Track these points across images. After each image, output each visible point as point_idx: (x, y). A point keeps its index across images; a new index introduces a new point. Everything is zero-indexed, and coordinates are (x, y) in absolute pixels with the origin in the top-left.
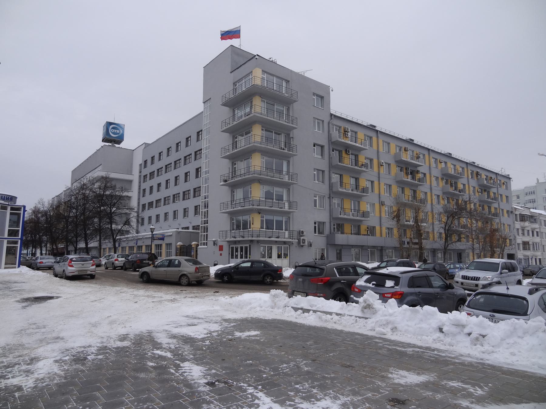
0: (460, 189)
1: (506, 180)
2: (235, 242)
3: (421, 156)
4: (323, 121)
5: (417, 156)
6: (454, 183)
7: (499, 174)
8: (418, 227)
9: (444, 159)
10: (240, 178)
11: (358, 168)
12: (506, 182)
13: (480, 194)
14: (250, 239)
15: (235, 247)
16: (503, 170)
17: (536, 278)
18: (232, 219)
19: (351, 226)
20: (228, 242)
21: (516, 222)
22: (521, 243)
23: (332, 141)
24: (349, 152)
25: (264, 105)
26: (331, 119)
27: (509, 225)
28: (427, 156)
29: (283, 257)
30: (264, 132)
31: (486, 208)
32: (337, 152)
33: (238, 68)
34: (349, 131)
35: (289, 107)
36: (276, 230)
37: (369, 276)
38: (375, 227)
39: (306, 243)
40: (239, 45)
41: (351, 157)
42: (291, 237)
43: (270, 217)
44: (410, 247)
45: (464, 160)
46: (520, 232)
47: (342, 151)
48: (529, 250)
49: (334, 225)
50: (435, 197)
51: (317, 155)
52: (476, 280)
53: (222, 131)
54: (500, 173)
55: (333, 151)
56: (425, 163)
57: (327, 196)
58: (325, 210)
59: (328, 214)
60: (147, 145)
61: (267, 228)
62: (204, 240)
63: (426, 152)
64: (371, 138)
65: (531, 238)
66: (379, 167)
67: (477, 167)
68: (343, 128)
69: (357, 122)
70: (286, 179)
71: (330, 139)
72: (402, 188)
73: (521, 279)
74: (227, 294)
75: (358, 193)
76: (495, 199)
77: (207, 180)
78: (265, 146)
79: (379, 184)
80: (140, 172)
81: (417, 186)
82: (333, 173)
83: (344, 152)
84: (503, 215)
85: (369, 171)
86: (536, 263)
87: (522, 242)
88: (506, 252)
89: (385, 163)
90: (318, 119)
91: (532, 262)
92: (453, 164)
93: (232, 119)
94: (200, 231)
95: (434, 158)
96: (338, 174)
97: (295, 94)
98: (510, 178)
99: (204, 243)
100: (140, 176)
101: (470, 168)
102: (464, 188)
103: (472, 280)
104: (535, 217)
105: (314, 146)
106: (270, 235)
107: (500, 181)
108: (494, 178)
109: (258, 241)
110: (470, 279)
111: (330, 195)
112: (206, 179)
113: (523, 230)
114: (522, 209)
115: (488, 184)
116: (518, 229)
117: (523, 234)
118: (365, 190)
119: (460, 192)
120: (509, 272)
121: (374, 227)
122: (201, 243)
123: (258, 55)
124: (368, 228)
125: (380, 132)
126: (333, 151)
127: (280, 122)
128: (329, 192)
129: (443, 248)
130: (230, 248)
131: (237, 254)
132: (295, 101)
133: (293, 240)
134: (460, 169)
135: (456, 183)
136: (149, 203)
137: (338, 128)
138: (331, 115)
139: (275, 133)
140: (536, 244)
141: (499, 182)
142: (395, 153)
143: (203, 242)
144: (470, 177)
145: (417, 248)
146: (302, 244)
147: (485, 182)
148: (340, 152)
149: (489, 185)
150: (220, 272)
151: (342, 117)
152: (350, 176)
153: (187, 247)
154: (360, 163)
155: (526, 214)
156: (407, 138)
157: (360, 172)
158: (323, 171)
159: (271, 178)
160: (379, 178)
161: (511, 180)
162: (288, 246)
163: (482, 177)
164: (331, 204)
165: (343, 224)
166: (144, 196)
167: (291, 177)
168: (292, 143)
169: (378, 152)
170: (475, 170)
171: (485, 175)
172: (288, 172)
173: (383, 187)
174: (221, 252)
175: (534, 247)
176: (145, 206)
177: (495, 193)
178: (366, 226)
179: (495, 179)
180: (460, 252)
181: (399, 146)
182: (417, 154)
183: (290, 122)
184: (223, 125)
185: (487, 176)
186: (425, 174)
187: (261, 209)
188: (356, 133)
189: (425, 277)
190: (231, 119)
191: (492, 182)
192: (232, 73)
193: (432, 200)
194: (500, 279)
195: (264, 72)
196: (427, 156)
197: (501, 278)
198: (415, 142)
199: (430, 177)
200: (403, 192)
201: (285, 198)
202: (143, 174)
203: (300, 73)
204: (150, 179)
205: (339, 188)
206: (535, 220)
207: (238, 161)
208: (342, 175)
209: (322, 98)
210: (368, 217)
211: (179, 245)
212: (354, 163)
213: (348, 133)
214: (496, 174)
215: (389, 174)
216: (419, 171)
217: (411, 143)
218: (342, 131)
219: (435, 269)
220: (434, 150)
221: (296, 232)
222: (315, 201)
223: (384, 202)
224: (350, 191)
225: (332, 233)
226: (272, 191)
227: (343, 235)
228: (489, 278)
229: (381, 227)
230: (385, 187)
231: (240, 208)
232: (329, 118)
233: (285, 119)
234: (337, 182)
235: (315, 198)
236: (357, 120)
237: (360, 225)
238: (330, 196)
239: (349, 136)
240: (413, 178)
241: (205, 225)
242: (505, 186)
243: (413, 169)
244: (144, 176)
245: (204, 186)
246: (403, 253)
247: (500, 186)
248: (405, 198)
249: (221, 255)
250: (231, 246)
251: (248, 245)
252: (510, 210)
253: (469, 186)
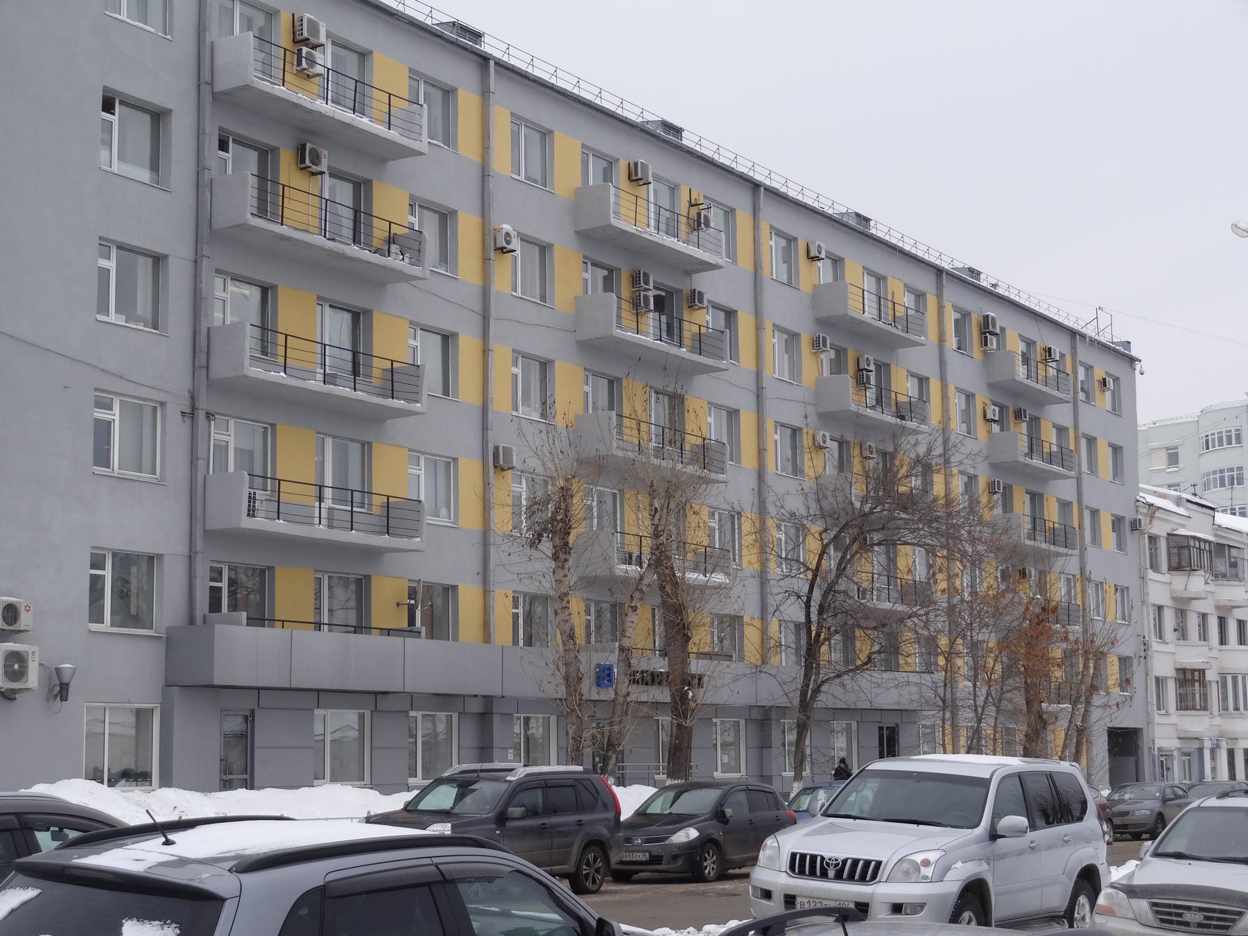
0: (901, 399)
1: (1116, 368)
3: (715, 216)
5: (694, 211)
6: (872, 367)
7: (1083, 336)
8: (668, 588)
9: (827, 241)
11: (366, 255)
12: (1116, 380)
13: (996, 428)
16: (1104, 321)
17: (1156, 854)
19: (319, 581)
21: (1151, 574)
22: (1172, 673)
23: (220, 86)
24: (316, 159)
27: (1121, 590)
28: (743, 219)
31: (1022, 504)
32: (253, 156)
37: (31, 893)
38: (455, 588)
39: (33, 678)
44: (621, 700)
45: (926, 257)
46: (1169, 620)
47: (275, 150)
48: (1205, 709)
49: (216, 575)
50: (775, 437)
51: (121, 158)
52: (863, 879)
54: (1090, 331)
55: (223, 146)
56: (732, 254)
58: (160, 483)
63: (740, 200)
64: (448, 93)
65: (1215, 653)
66: (486, 260)
67: (990, 294)
68: (285, 19)
72: (611, 382)
73: (1101, 862)
75: (359, 395)
76: (1063, 457)
79: (486, 351)
81: (689, 371)
82: (218, 271)
83: (286, 159)
84: (1096, 539)
85: (428, 274)
86: (1232, 775)
87: (1178, 670)
88: (1100, 722)
89: (525, 240)
91: (1214, 769)
92: (871, 273)
95: (779, 233)
96: (250, 282)
98: (1132, 360)
101: (953, 295)
102: (921, 398)
103: (839, 876)
104: (1234, 552)
105: (108, 106)
107: (1089, 369)
108: (1062, 356)
110: (831, 873)
111: (193, 398)
113: (1181, 614)
114: (1181, 511)
115: (1034, 384)
116: (1160, 608)
117: (1182, 632)
118: (706, 455)
119: (903, 418)
120: (1033, 827)
121: (449, 591)
124: (412, 593)
125: (500, 64)
128: (188, 386)
129: (796, 702)
134: (907, 300)
135: (883, 369)
137: (260, 20)
140: (1235, 679)
141: (1081, 373)
142: (577, 190)
144: (952, 341)
145: (656, 705)
147: (1021, 371)
148: (266, 155)
149: (1040, 387)
154: (380, 231)
155: (1194, 538)
156: (849, 211)
157: (379, 280)
158: (158, 260)
160: (485, 317)
161: (1138, 367)
163: (1008, 348)
164: (201, 453)
165: (271, 569)
169: (485, 174)
170: (979, 308)
171: (1023, 339)
173: (505, 369)
175: (1225, 698)
177: (1066, 429)
178: (406, 584)
179: (1068, 359)
180: (889, 722)
181: (599, 156)
182: (691, 205)
185: (1030, 344)
186: (730, 314)
188: (364, 56)
189: (428, 884)
191: (1052, 372)
193: (761, 451)
194: (985, 866)
196: (743, 219)
197: (990, 859)
198: (688, 140)
199: (759, 328)
200: (614, 401)
205: (247, 362)
206: (1234, 565)
208: (274, 287)
210: (413, 532)
212: (350, 224)
213: (318, 55)
214: (1073, 334)
215: (543, 298)
216: (701, 294)
217: (464, 48)
218: (283, 37)
219: (723, 813)
220: (784, 190)
222: (103, 429)
223: (508, 452)
224: (316, 384)
225: (199, 621)
227: (264, 633)
228: (926, 863)
229: (486, 592)
230: (518, 371)
234: (237, 327)
236: (599, 95)
237: (368, 578)
238: (193, 408)
240: (672, 331)
242: (1108, 394)
243: (671, 282)
246: (580, 730)
247: (1087, 393)
248: (620, 433)
252: (1129, 515)
253: (944, 387)
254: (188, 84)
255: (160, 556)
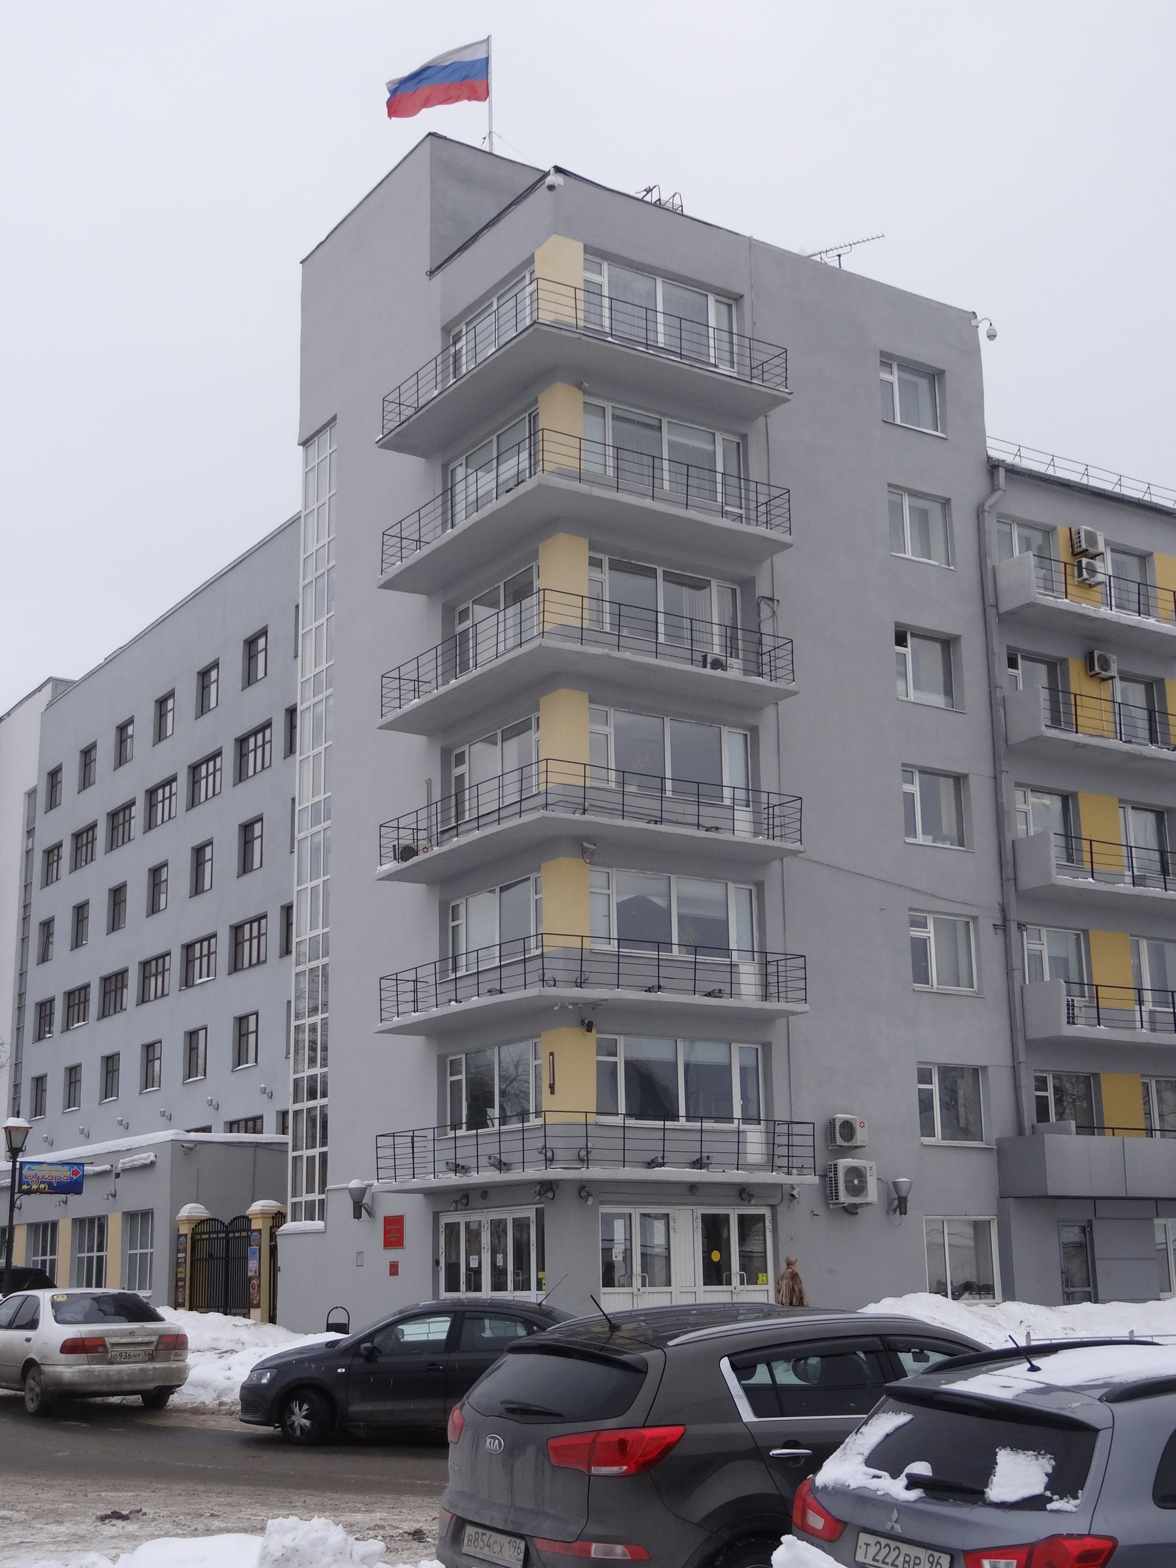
2: (464, 1197)
4: (946, 503)
10: (477, 834)
14: (534, 1173)
15: (467, 1224)
18: (446, 1066)
19: (1146, 1087)
20: (431, 1194)
24: (1105, 665)
25: (603, 430)
26: (994, 488)
29: (735, 1280)
30: (605, 575)
32: (1042, 670)
33: (464, 248)
34: (1101, 547)
35: (744, 437)
36: (689, 1118)
37: (903, 1418)
39: (873, 1193)
40: (486, 134)
41: (1124, 692)
42: (783, 1162)
43: (653, 1050)
47: (1064, 661)
49: (1041, 1084)
51: (917, 687)
53: (388, 585)
55: (1012, 663)
57: (989, 919)
58: (978, 996)
59: (998, 1023)
60: (60, 687)
61: (638, 1110)
62: (310, 1190)
68: (1062, 535)
69: (1147, 498)
70: (742, 827)
71: (991, 599)
74: (321, 1509)
77: (321, 856)
78: (606, 651)
80: (30, 833)
82: (1018, 785)
83: (1076, 669)
90: (914, 494)
93: (439, 511)
94: (288, 1138)
96: (1050, 792)
97: (777, 361)
99: (310, 1205)
100: (28, 853)
105: (901, 640)
106: (653, 1148)
109: (583, 1188)
111: (1003, 910)
112: (315, 850)
122: (294, 1205)
123: (558, 170)
126: (1012, 663)
127: (692, 514)
128: (999, 899)
130: (442, 1229)
131: (474, 1264)
132: (777, 401)
133: (794, 1179)
136: (69, 994)
137: (1037, 538)
138: (993, 466)
139: (668, 577)
143: (306, 1197)
146: (844, 1198)
148: (1055, 667)
150: (271, 1381)
151: (1094, 483)
152: (1121, 801)
153: (227, 1229)
158: (959, 780)
159: (652, 827)
162: (766, 1211)
164: (1016, 963)
166: (44, 958)
167: (765, 821)
168: (766, 628)
172: (753, 789)
174: (394, 1254)
176: (51, 1014)
183: (753, 515)
184: (392, 551)
187: (595, 1005)
188: (1144, 558)
190: (433, 514)
192: (439, 277)
195: (595, 254)
201: (737, 936)
202: (43, 841)
203: (817, 258)
204: (75, 866)
205: (1054, 870)
207: (471, 742)
208: (1074, 795)
209: (935, 376)
211: (189, 1220)
212: (1145, 724)
213: (1098, 564)
218: (1061, 551)
221: (808, 1129)
222: (920, 947)
224: (1125, 887)
225: (1028, 1132)
226: (661, 902)
227: (1095, 1140)
231: (475, 1002)
232: (977, 483)
233: (719, 496)
235: (917, 933)
238: (1005, 919)
239: (1100, 578)
241: (312, 1104)
244: (49, 852)
245: (309, 885)
249: (394, 1269)
250: (445, 1219)
251: (529, 1212)
254: (975, 609)
255: (985, 1068)
